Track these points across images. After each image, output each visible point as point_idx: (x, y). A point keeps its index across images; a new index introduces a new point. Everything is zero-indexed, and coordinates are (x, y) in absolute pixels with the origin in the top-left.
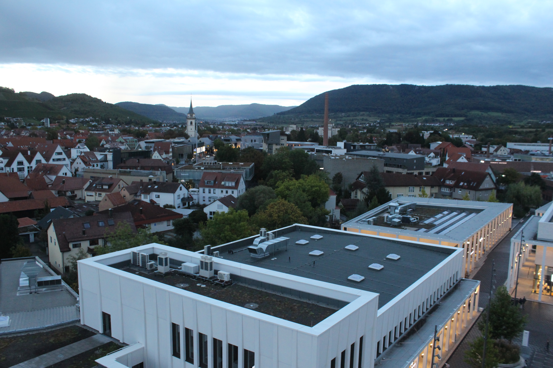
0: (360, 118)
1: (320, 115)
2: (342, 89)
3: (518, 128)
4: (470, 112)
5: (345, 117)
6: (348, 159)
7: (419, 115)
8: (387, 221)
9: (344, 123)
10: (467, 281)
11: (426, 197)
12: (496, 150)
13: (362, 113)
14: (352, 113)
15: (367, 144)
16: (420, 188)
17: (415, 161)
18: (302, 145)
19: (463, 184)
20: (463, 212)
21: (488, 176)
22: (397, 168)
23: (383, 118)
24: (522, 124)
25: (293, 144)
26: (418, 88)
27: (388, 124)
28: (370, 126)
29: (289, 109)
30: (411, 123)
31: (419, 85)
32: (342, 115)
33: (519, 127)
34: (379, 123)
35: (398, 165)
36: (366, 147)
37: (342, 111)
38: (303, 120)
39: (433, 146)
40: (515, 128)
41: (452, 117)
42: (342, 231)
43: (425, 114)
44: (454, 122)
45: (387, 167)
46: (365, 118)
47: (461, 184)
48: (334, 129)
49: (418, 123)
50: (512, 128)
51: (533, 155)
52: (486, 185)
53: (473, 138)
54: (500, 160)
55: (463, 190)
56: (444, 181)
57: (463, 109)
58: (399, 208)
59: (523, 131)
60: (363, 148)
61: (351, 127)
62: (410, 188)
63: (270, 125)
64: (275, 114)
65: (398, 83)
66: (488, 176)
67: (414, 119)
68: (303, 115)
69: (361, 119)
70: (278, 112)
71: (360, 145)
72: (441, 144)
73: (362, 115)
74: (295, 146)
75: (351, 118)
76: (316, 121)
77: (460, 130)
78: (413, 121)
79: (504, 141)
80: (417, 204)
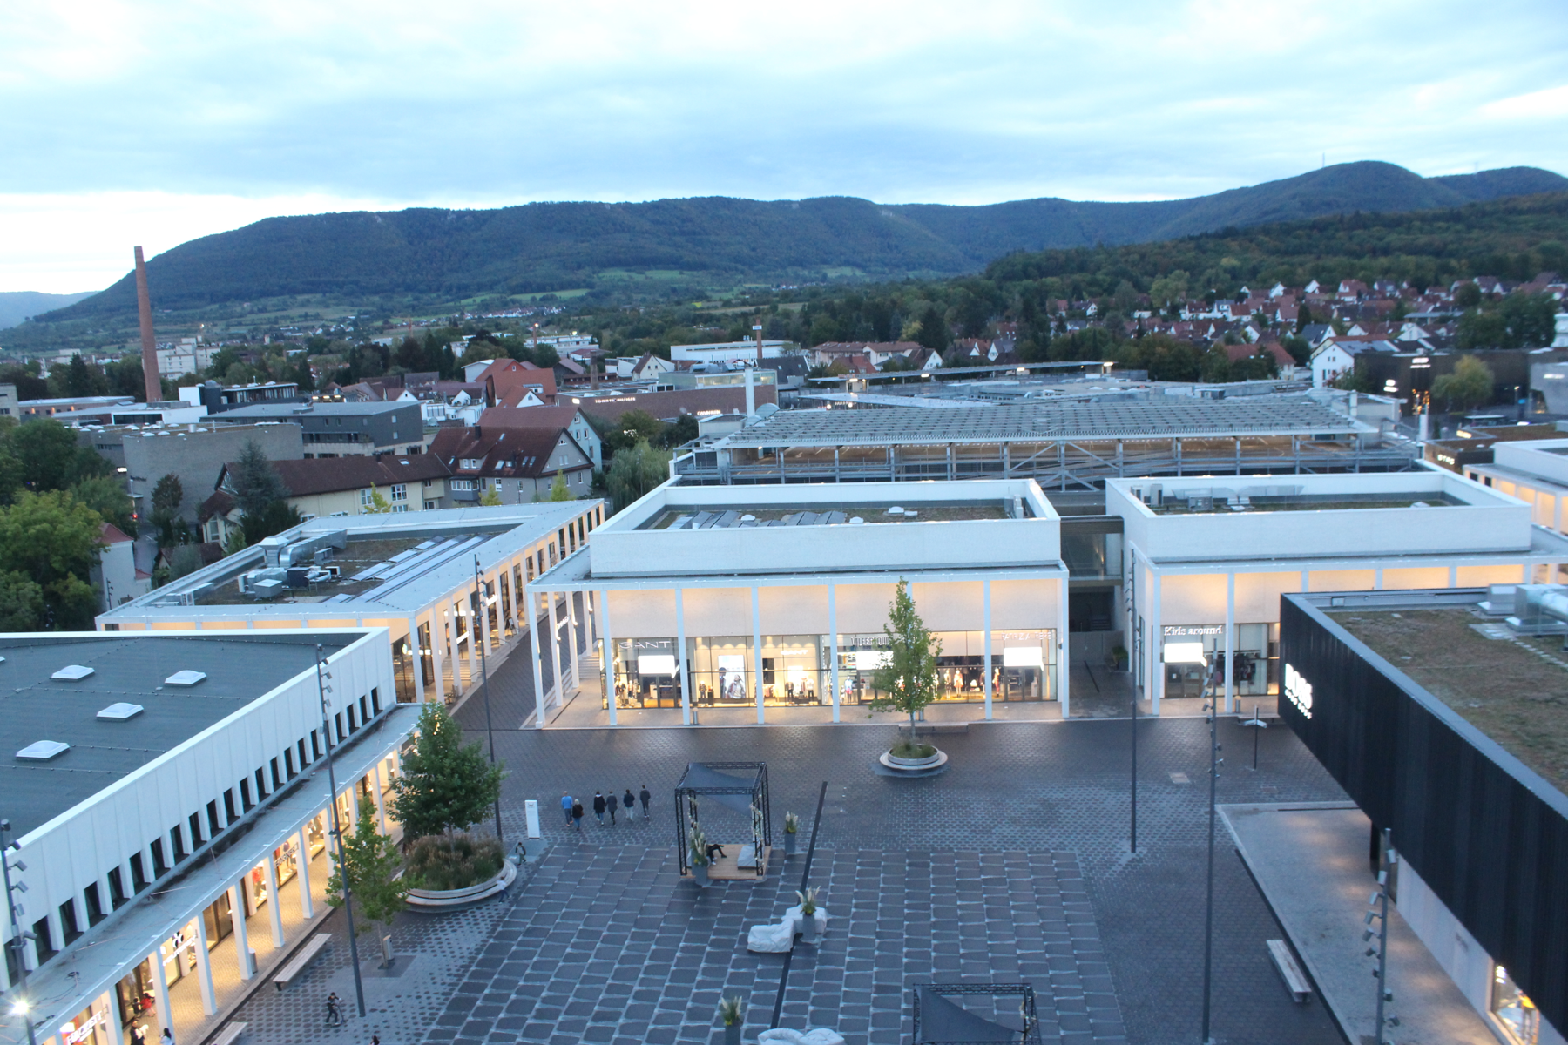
0: (295, 312)
1: (176, 313)
2: (235, 232)
3: (716, 308)
4: (601, 275)
5: (251, 312)
6: (195, 433)
7: (463, 291)
8: (246, 589)
9: (249, 331)
10: (409, 709)
11: (385, 511)
12: (638, 370)
13: (301, 298)
14: (275, 300)
15: (271, 384)
16: (394, 490)
17: (394, 420)
18: (79, 408)
19: (504, 465)
20: (476, 535)
21: (563, 437)
22: (347, 444)
23: (363, 309)
24: (727, 296)
25: (51, 407)
26: (454, 216)
27: (379, 323)
28: (327, 333)
29: (74, 302)
30: (444, 316)
31: (456, 209)
32: (243, 308)
33: (719, 304)
34: (354, 324)
35: (349, 435)
36: (268, 394)
37: (241, 296)
38: (123, 331)
39: (473, 372)
40: (708, 308)
41: (553, 290)
42: (101, 633)
43: (480, 288)
44: (558, 302)
45: (319, 445)
46: (311, 311)
47: (499, 465)
48: (203, 352)
49: (462, 314)
50: (702, 309)
51: (701, 371)
52: (561, 459)
53: (592, 342)
54: (620, 393)
55: (504, 480)
56: (456, 464)
57: (579, 267)
58: (290, 551)
59: (726, 315)
60: (257, 396)
61: (271, 341)
62: (363, 493)
63: (13, 355)
64: (27, 318)
65: (399, 206)
66: (563, 437)
67: (452, 304)
68: (122, 317)
69: (300, 316)
70: (38, 313)
71: (247, 391)
72: (490, 366)
73: (303, 305)
74: (58, 411)
75: (272, 315)
76: (166, 333)
77: (571, 323)
78: (450, 310)
79: (666, 343)
80: (349, 533)
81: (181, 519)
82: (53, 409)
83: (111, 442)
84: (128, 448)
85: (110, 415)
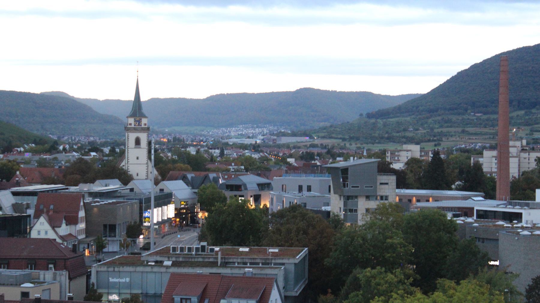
1: (485, 117)
18: (436, 199)
63: (348, 145)
68: (439, 118)
74: (418, 201)
76: (476, 134)
81: (359, 276)
82: (414, 199)
83: (485, 236)
84: (504, 242)
85: (473, 208)
